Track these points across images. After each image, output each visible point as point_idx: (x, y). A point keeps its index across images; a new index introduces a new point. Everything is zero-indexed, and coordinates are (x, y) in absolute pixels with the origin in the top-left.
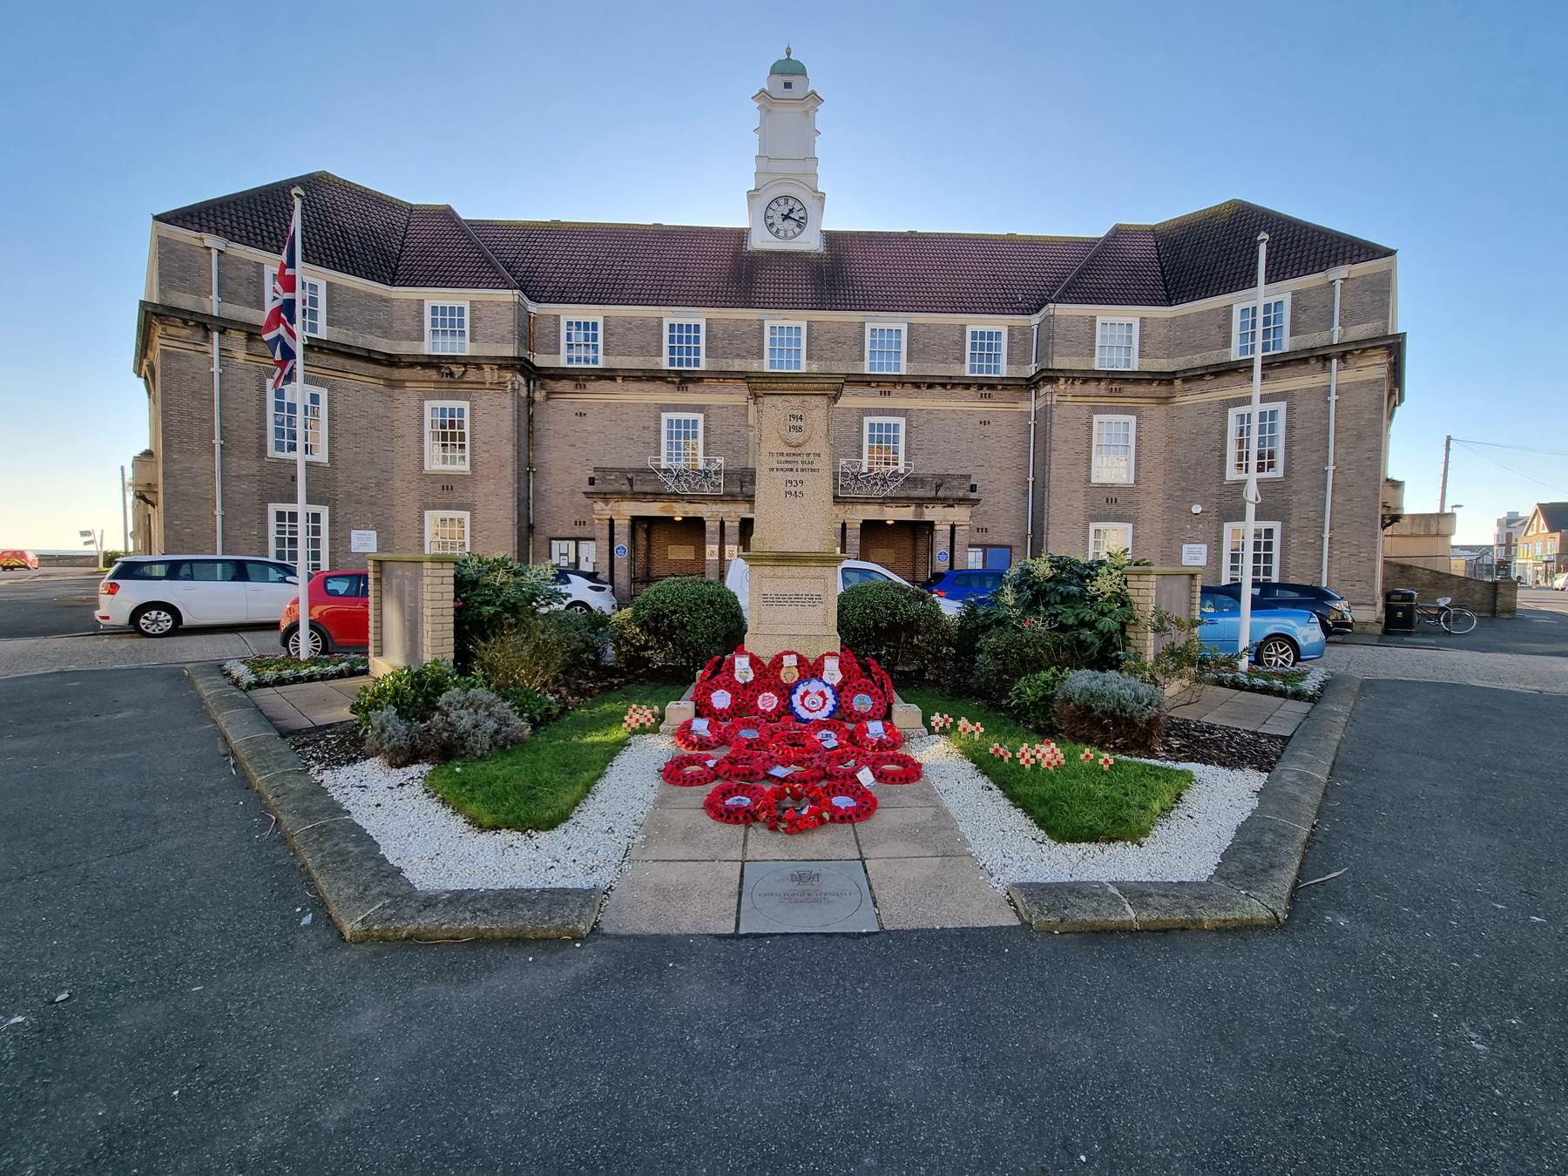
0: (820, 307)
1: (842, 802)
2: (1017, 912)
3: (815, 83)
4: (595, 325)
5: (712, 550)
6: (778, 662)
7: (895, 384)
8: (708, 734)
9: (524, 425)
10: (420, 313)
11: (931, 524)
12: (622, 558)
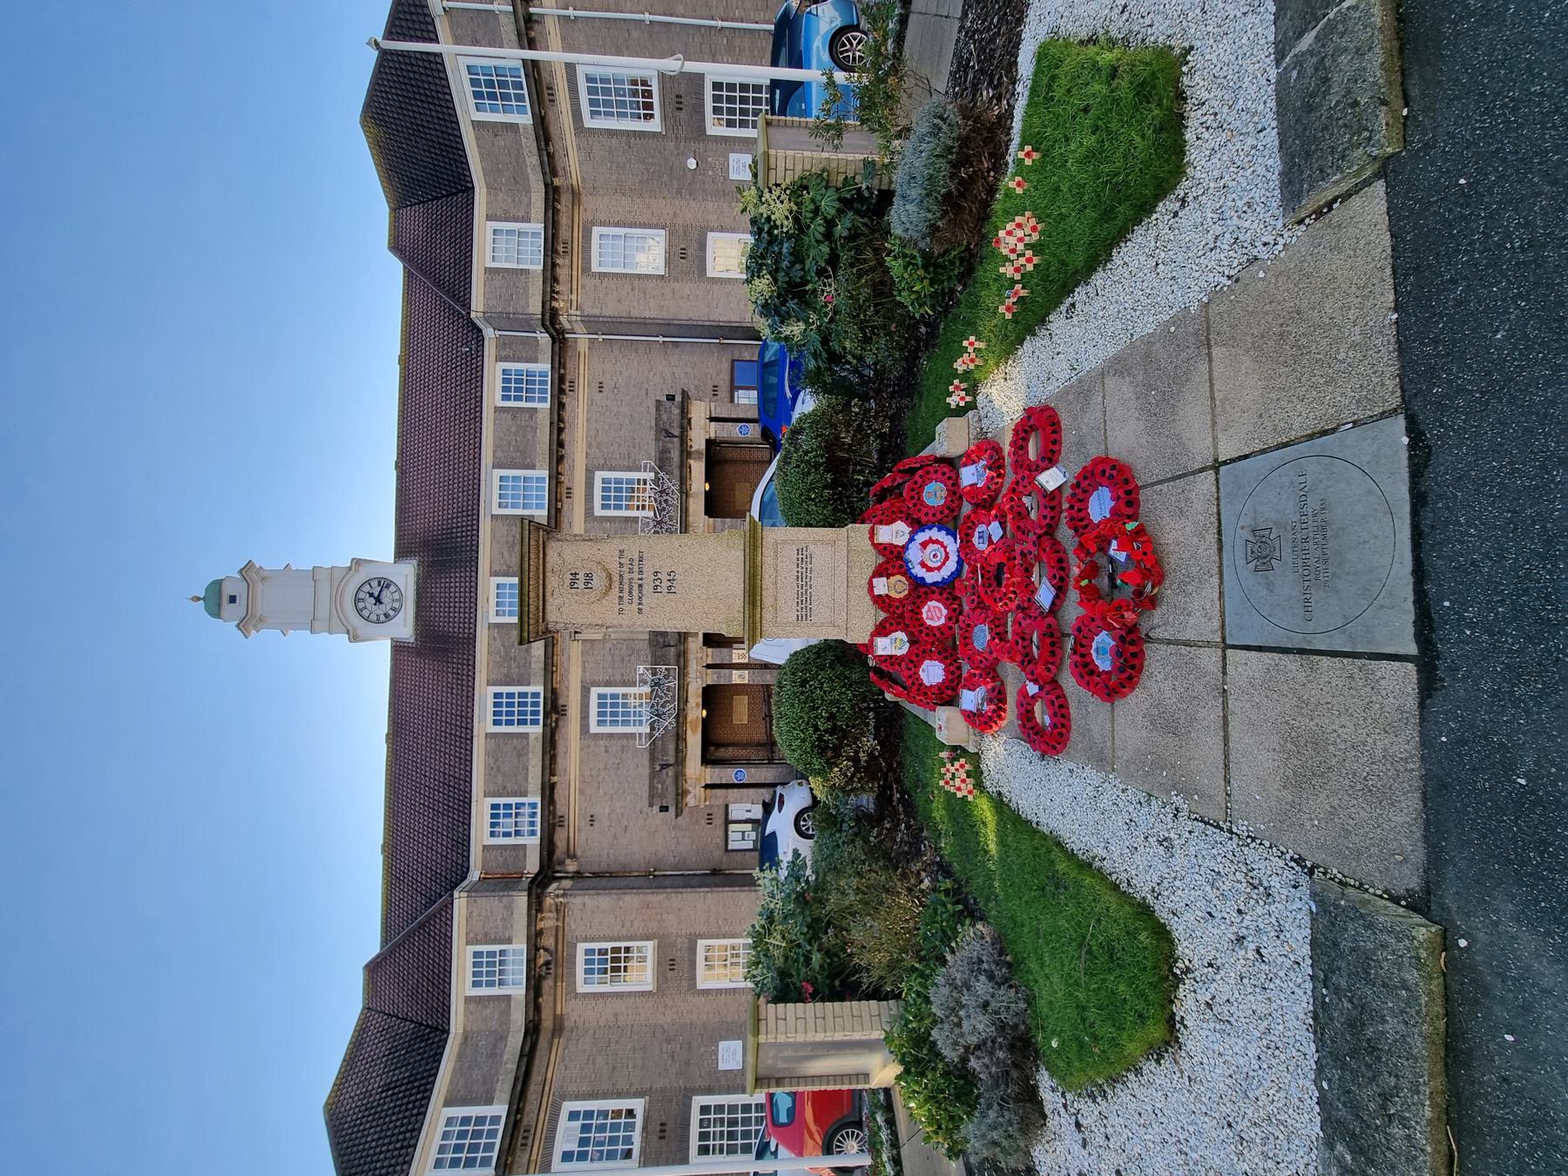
1: (1100, 506)
3: (229, 569)
4: (494, 807)
5: (738, 677)
6: (881, 602)
7: (558, 483)
8: (981, 691)
9: (603, 882)
10: (479, 999)
11: (709, 442)
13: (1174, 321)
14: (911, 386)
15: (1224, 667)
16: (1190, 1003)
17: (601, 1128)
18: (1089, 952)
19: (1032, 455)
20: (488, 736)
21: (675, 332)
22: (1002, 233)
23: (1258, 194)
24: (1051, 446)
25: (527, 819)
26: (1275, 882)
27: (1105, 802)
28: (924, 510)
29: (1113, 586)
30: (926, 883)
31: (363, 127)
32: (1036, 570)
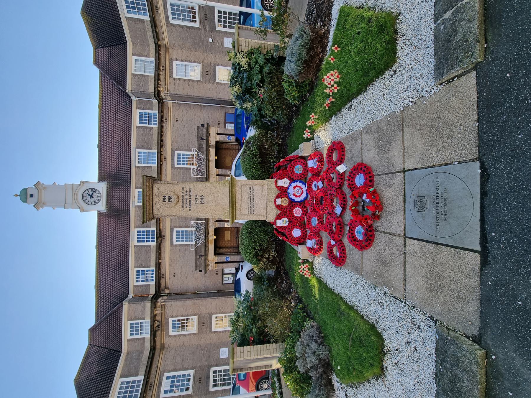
0: (129, 184)
1: (360, 180)
2: (464, 74)
3: (30, 184)
4: (138, 271)
6: (279, 207)
7: (161, 155)
9: (178, 297)
10: (133, 340)
11: (217, 142)
12: (230, 258)
13: (389, 116)
15: (405, 244)
16: (389, 362)
17: (178, 381)
18: (353, 339)
19: (334, 159)
21: (204, 102)
22: (325, 77)
23: (425, 72)
25: (150, 275)
26: (422, 324)
27: (359, 286)
29: (364, 209)
30: (293, 304)
31: (82, 16)
32: (335, 200)
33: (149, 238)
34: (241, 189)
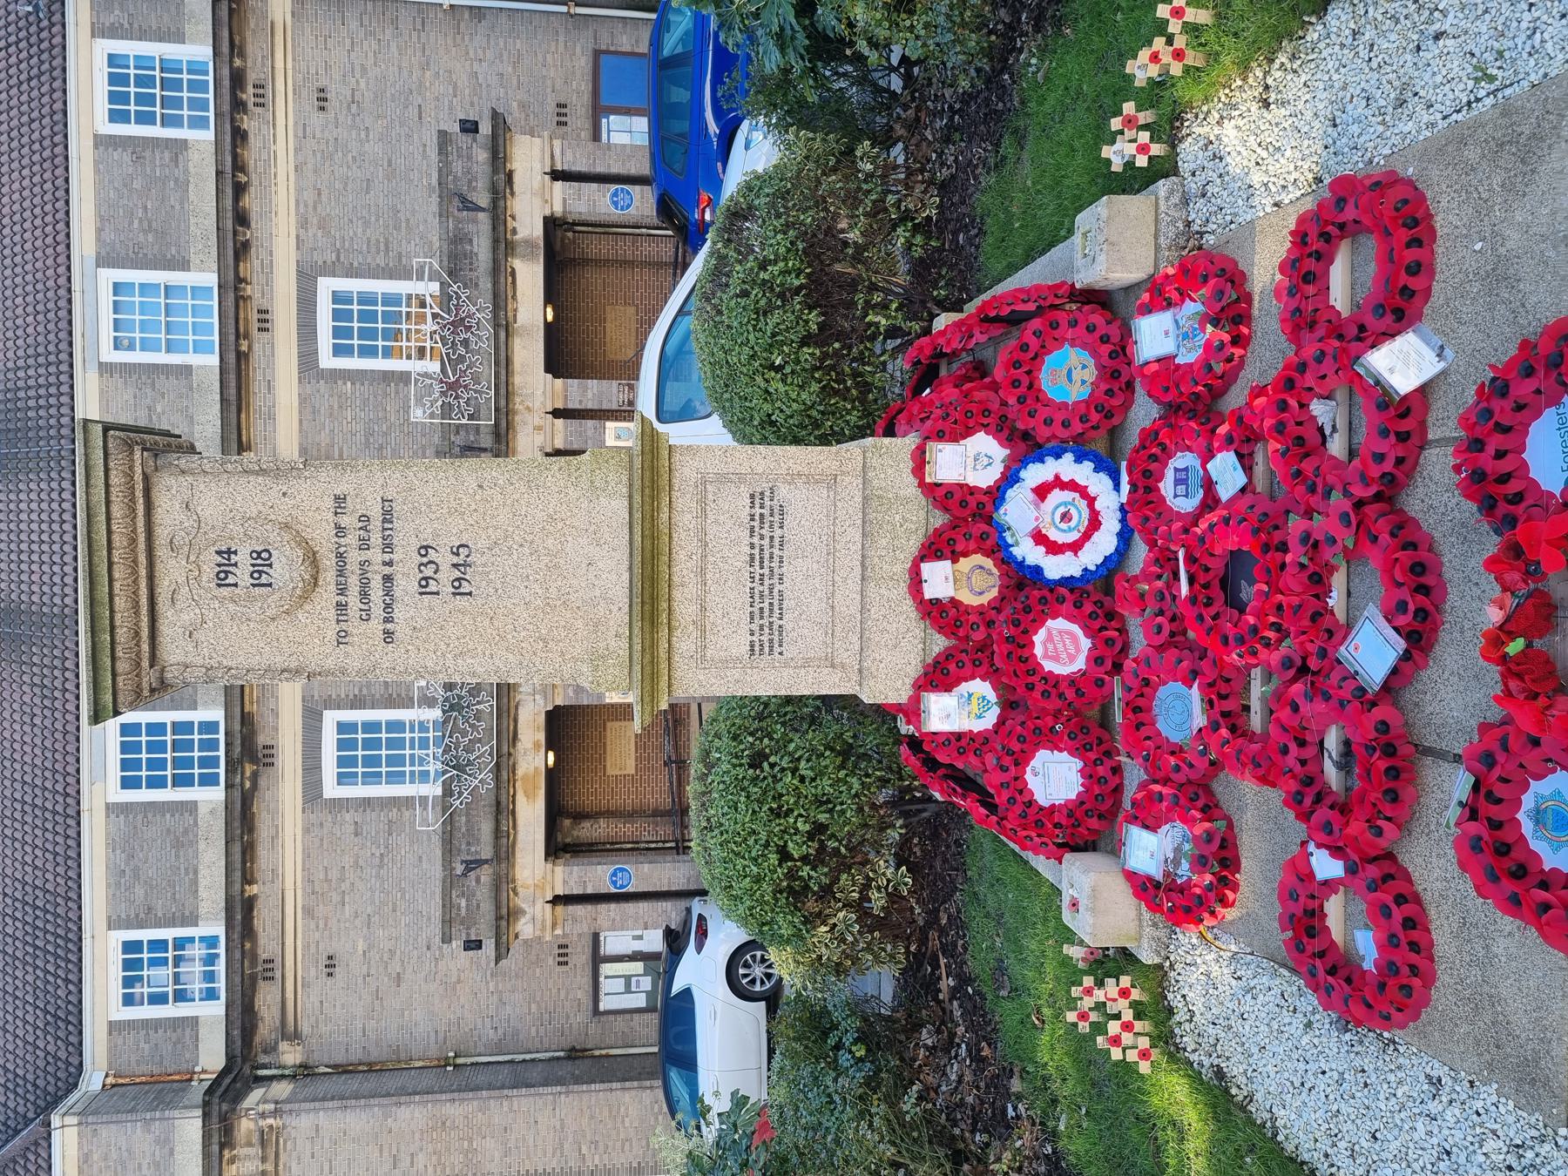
4: (129, 947)
6: (938, 613)
7: (240, 299)
9: (354, 1083)
11: (551, 224)
14: (994, 116)
20: (112, 809)
24: (1404, 278)
28: (1044, 413)
32: (1338, 581)
33: (188, 763)
34: (703, 502)
